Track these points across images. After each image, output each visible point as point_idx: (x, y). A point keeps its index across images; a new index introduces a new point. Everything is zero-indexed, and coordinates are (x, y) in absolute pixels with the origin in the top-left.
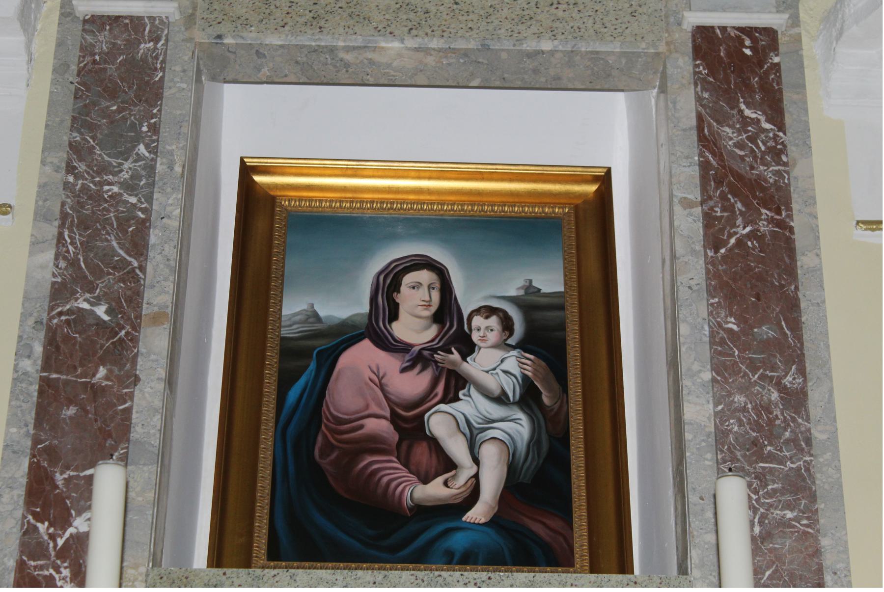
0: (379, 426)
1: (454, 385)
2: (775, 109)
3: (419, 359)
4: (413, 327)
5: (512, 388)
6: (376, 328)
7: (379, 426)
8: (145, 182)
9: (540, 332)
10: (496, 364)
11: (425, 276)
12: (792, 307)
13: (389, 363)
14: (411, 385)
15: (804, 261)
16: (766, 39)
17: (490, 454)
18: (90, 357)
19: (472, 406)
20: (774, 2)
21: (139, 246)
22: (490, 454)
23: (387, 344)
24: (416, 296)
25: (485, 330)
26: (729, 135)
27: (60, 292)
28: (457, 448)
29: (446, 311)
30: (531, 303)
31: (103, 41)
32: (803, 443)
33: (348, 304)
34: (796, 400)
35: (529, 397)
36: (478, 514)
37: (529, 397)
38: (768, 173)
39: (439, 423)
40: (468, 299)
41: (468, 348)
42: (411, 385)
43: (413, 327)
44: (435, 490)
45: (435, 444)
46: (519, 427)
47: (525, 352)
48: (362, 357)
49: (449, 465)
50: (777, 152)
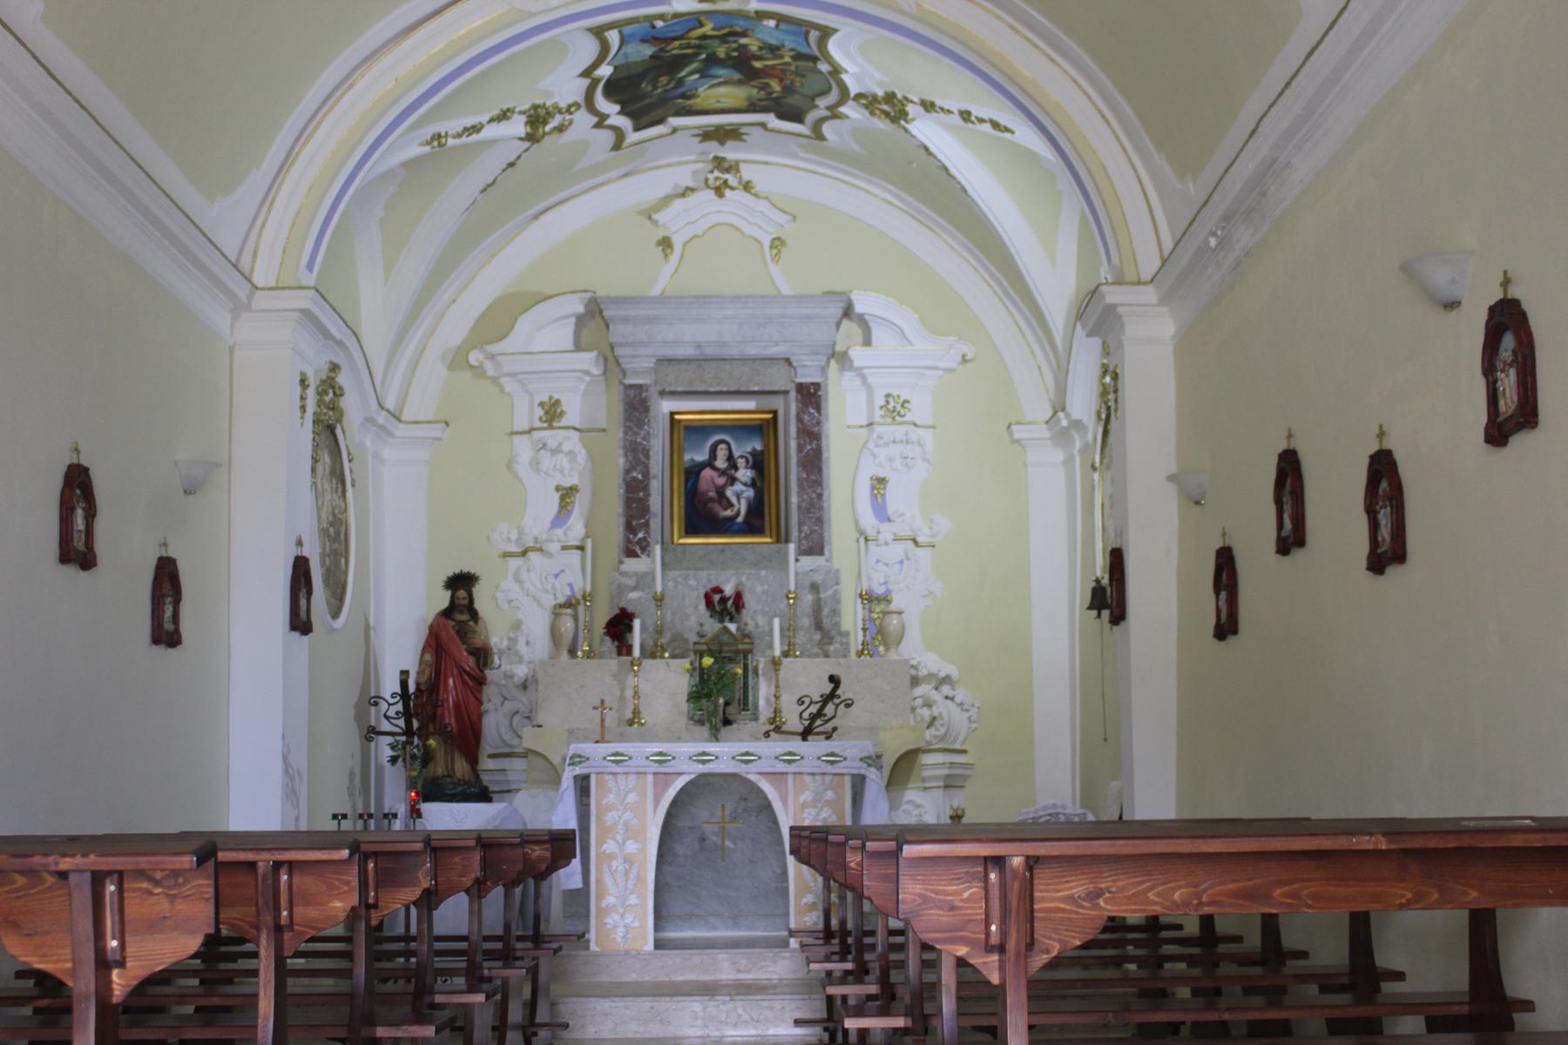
0: (712, 494)
1: (733, 480)
2: (818, 409)
3: (722, 473)
4: (721, 463)
5: (749, 481)
6: (710, 463)
7: (712, 494)
8: (647, 437)
9: (758, 463)
10: (744, 474)
11: (723, 446)
12: (820, 470)
13: (714, 474)
14: (721, 481)
15: (825, 455)
16: (817, 386)
17: (743, 501)
18: (638, 490)
19: (738, 487)
20: (598, 1018)
21: (647, 457)
22: (743, 501)
23: (714, 468)
24: (722, 452)
25: (741, 463)
26: (806, 418)
27: (628, 471)
28: (734, 500)
29: (730, 457)
30: (754, 453)
31: (632, 393)
32: (821, 508)
33: (701, 456)
34: (820, 496)
35: (753, 484)
36: (740, 519)
37: (753, 484)
38: (816, 429)
39: (729, 493)
40: (736, 453)
41: (736, 469)
42: (721, 481)
43: (721, 463)
44: (729, 513)
45: (728, 500)
46: (750, 493)
47: (691, 783)
48: (707, 473)
49: (731, 505)
50: (819, 423)
